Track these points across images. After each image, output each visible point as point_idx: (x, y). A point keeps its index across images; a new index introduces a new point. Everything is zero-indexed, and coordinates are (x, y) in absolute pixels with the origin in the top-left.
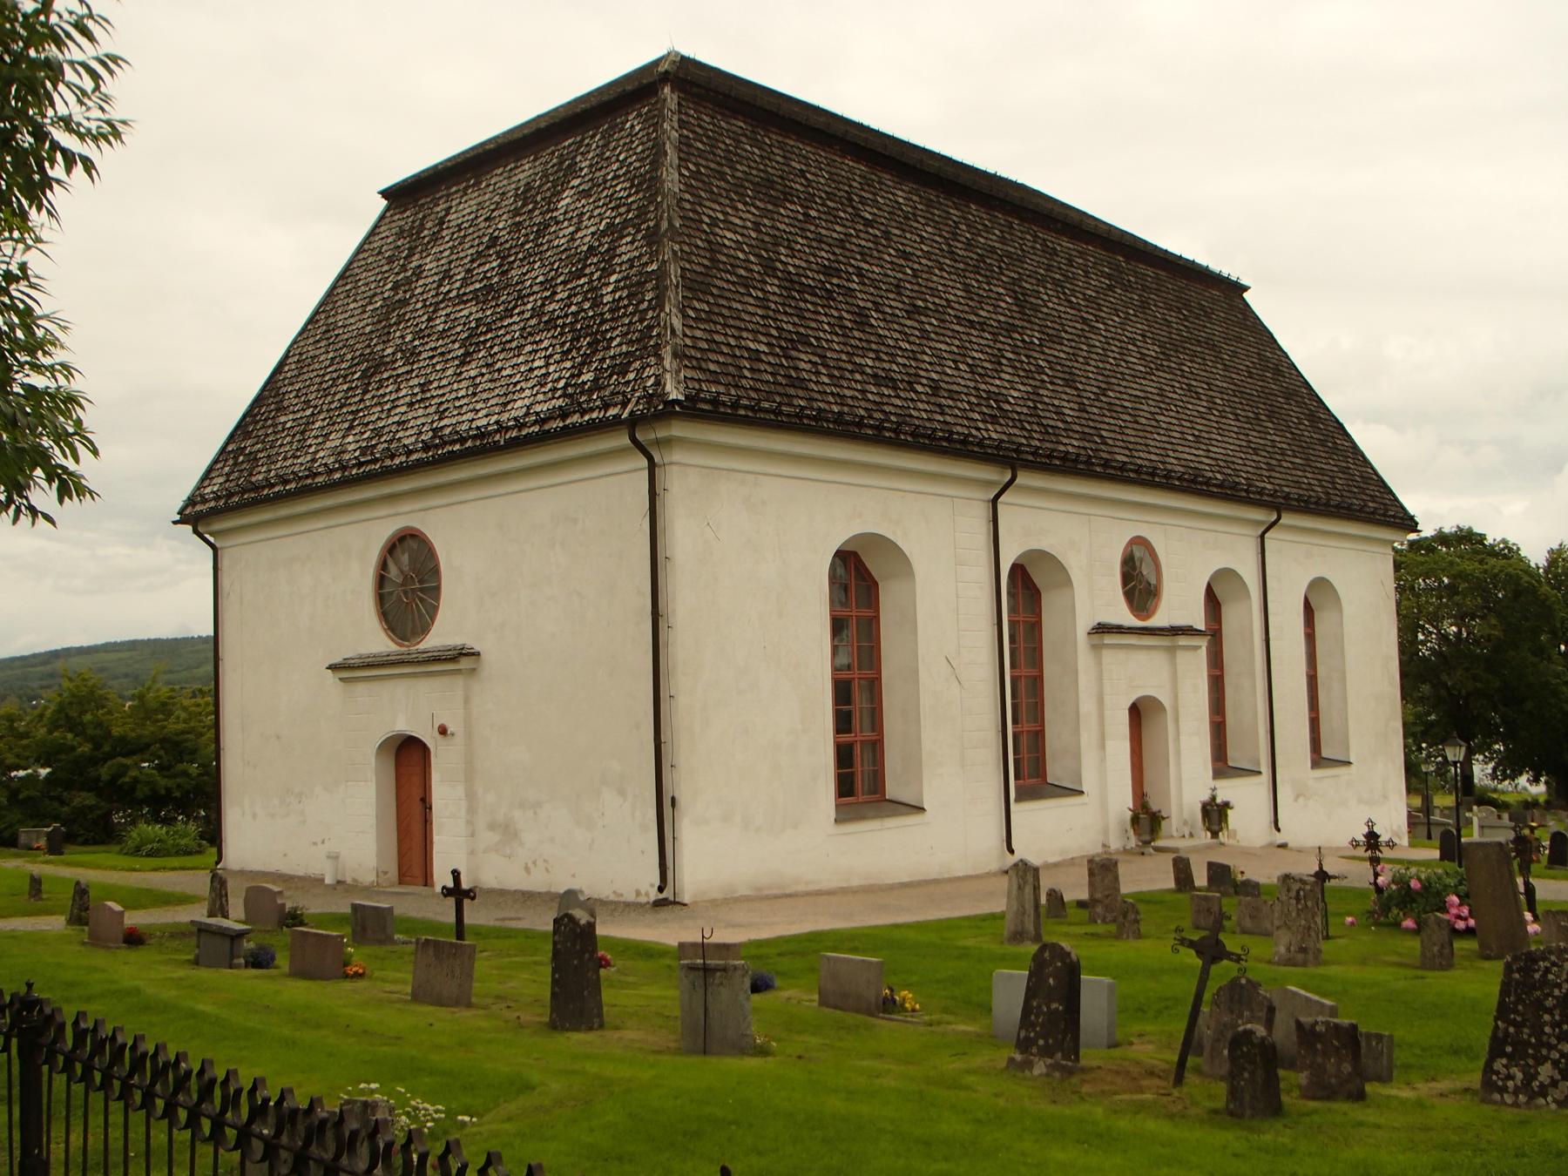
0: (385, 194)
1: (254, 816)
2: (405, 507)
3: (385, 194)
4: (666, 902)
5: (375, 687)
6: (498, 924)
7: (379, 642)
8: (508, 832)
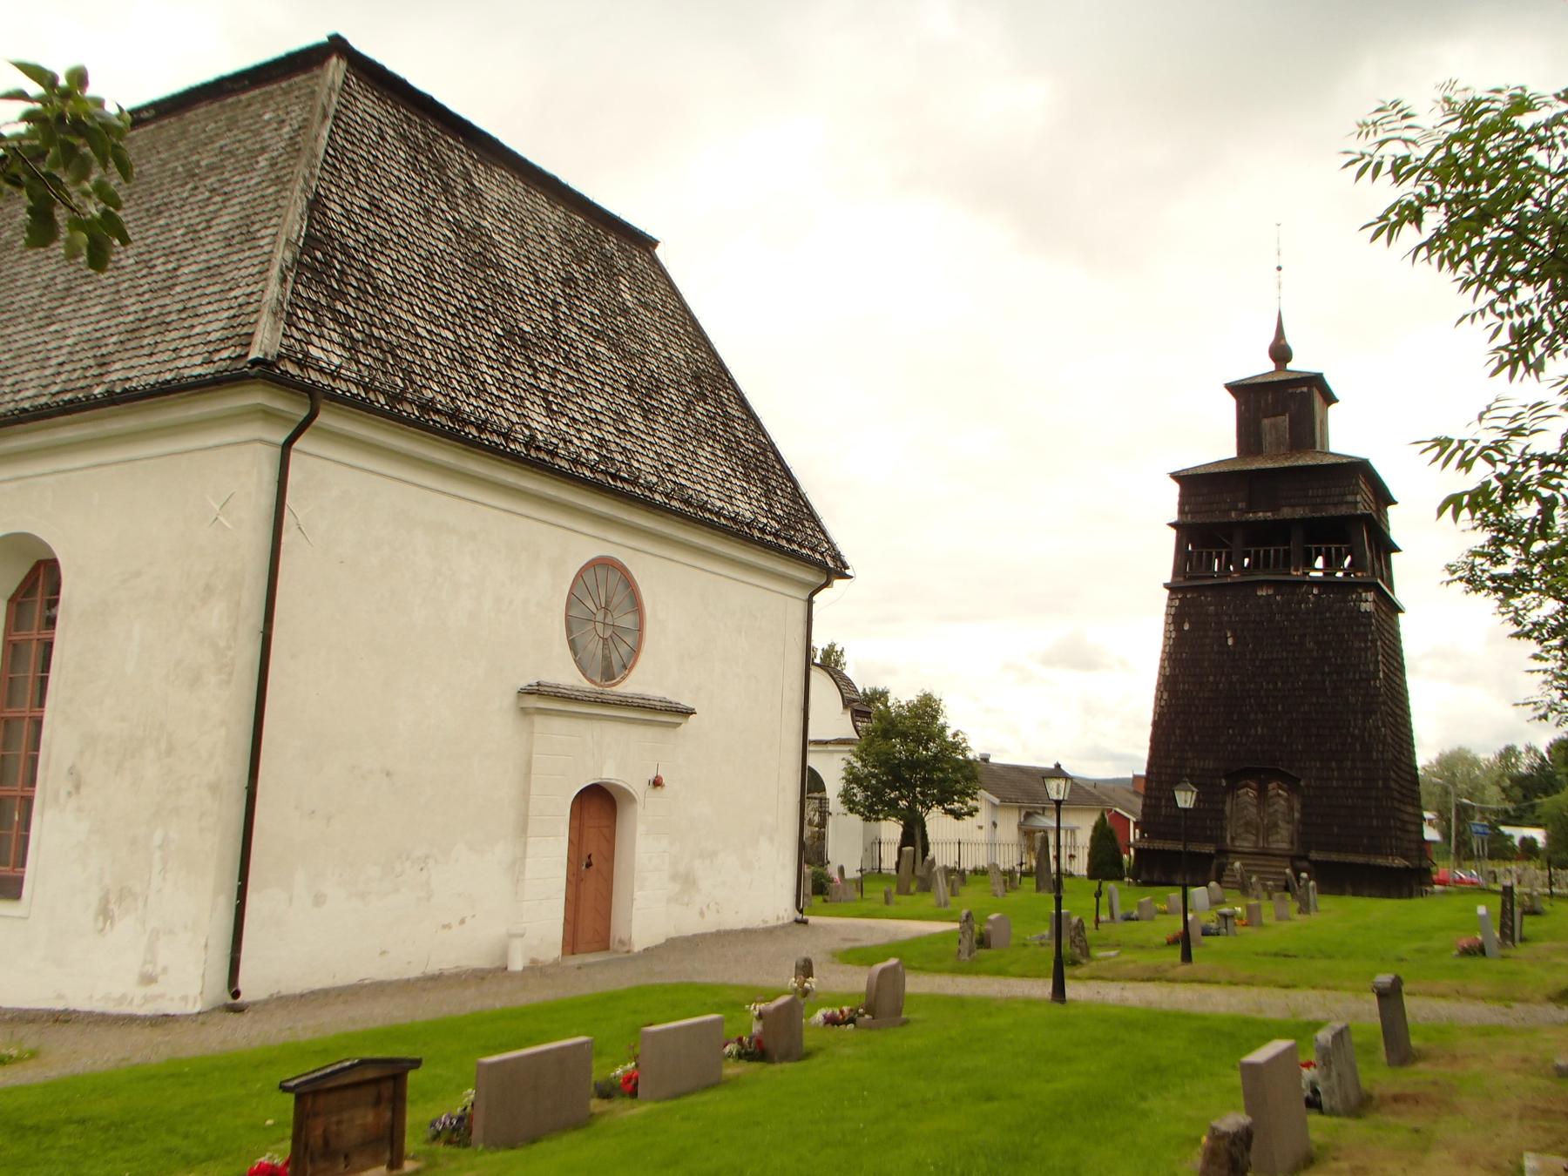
2: (615, 536)
4: (234, 1004)
6: (848, 945)
8: (687, 881)
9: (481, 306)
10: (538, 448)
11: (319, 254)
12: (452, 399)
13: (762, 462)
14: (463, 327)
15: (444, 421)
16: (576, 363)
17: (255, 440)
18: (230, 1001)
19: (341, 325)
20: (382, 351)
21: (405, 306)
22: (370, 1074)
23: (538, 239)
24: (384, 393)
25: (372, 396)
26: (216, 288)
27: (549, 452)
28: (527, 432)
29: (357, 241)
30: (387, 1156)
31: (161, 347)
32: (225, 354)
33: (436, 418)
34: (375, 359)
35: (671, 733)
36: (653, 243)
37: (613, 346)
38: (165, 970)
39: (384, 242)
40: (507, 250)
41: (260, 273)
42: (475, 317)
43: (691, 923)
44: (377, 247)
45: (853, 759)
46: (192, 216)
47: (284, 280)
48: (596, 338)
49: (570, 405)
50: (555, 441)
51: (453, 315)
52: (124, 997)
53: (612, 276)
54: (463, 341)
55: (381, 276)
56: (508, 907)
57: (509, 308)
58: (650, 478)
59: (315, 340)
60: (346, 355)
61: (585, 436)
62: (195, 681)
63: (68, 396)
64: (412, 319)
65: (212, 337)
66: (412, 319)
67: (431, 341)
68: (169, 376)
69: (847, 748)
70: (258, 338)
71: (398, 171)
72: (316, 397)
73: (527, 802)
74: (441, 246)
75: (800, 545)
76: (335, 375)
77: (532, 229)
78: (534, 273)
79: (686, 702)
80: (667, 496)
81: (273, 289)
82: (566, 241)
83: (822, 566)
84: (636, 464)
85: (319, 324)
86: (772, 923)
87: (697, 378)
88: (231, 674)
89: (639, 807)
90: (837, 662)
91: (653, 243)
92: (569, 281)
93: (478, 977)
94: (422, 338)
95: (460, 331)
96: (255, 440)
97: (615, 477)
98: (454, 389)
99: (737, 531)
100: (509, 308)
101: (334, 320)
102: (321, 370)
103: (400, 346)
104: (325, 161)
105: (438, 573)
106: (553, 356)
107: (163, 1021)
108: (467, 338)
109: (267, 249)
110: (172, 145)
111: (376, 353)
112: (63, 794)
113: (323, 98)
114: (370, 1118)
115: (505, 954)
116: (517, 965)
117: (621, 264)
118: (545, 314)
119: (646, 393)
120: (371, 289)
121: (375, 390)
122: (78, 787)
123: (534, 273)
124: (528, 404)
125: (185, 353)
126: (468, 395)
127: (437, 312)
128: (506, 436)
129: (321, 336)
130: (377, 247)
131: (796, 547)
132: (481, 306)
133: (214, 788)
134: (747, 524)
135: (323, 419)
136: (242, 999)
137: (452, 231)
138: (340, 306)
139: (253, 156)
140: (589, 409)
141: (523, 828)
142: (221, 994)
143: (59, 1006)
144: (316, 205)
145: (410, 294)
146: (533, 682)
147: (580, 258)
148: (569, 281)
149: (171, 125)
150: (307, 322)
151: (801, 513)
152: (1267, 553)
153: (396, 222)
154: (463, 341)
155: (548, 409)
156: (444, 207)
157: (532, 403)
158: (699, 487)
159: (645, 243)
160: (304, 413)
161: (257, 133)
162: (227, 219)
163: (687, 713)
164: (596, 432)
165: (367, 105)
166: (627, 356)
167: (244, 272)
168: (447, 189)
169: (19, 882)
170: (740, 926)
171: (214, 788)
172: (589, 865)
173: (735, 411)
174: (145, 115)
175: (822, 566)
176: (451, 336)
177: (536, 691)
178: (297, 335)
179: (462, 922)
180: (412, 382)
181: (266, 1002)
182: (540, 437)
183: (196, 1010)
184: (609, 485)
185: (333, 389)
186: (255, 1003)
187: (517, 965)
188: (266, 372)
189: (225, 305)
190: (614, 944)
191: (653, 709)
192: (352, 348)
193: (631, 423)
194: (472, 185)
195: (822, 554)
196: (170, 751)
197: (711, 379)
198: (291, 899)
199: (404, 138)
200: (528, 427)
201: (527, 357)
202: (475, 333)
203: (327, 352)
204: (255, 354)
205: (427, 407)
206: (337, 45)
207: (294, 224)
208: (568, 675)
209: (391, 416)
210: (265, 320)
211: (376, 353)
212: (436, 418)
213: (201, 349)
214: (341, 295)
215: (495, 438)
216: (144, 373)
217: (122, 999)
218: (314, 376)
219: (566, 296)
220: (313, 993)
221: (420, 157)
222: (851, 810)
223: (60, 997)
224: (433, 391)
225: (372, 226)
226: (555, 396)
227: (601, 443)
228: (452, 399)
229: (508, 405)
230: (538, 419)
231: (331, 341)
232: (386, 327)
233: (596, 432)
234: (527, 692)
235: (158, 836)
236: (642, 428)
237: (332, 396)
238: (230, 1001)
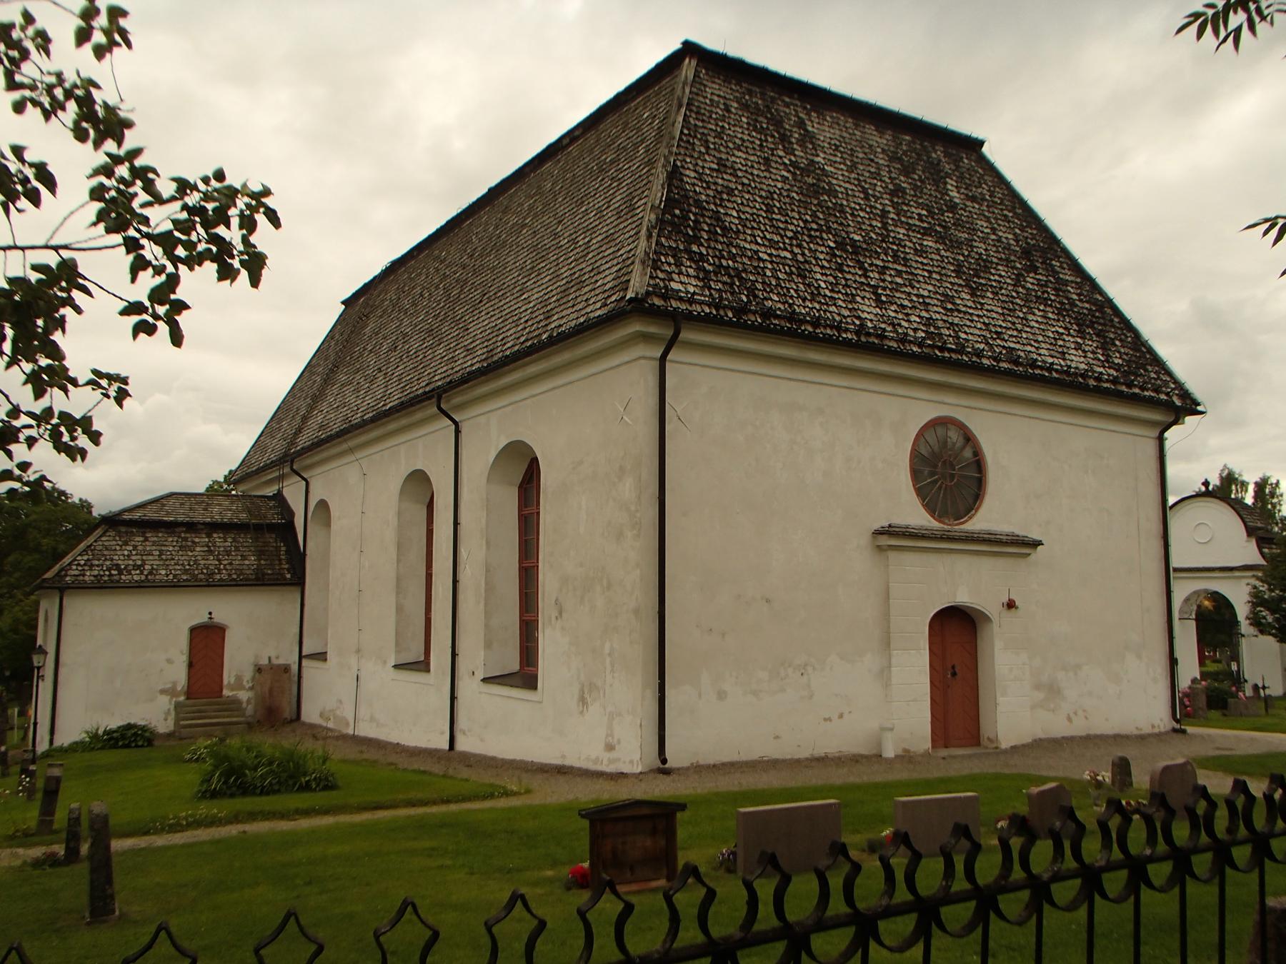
0: (343, 303)
1: (721, 695)
2: (951, 398)
3: (343, 303)
4: (663, 769)
5: (932, 558)
6: (1218, 753)
7: (916, 516)
8: (1052, 691)
9: (815, 226)
10: (868, 334)
11: (677, 212)
12: (790, 305)
13: (1099, 316)
14: (800, 246)
15: (783, 323)
16: (904, 259)
17: (640, 358)
19: (696, 262)
20: (730, 276)
21: (749, 238)
22: (646, 811)
23: (867, 162)
24: (732, 308)
25: (722, 313)
27: (877, 336)
28: (858, 322)
29: (707, 195)
30: (665, 872)
31: (579, 300)
32: (613, 298)
33: (776, 322)
34: (724, 283)
35: (1022, 562)
36: (981, 143)
37: (940, 239)
38: (619, 742)
39: (730, 192)
40: (840, 179)
42: (810, 236)
43: (1057, 726)
44: (725, 196)
45: (1258, 583)
46: (600, 202)
47: (649, 236)
49: (898, 295)
50: (883, 326)
51: (790, 238)
52: (597, 758)
53: (938, 178)
54: (800, 258)
55: (728, 219)
56: (885, 707)
57: (841, 224)
58: (977, 346)
59: (675, 277)
60: (700, 284)
61: (913, 318)
62: (620, 536)
63: (529, 344)
64: (754, 247)
65: (607, 287)
66: (754, 247)
67: (771, 262)
68: (582, 320)
69: (1249, 574)
70: (632, 283)
71: (740, 134)
72: (678, 320)
73: (889, 622)
74: (779, 185)
75: (1143, 389)
76: (691, 301)
77: (861, 155)
78: (864, 191)
79: (1035, 536)
80: (995, 359)
81: (643, 243)
82: (893, 158)
83: (1168, 406)
84: (963, 336)
85: (679, 264)
86: (1147, 730)
87: (1026, 253)
89: (995, 626)
90: (1273, 495)
91: (981, 143)
92: (897, 191)
93: (856, 759)
94: (764, 261)
95: (796, 250)
96: (640, 358)
97: (942, 349)
98: (792, 297)
99: (1072, 383)
100: (841, 224)
101: (690, 259)
102: (681, 299)
103: (745, 271)
104: (680, 139)
105: (831, 443)
106: (883, 257)
107: (622, 775)
108: (803, 254)
110: (591, 151)
111: (725, 279)
113: (679, 92)
114: (649, 843)
115: (879, 744)
116: (889, 753)
117: (947, 168)
118: (874, 223)
119: (974, 277)
120: (720, 227)
121: (725, 307)
122: (560, 613)
123: (864, 191)
124: (858, 299)
126: (804, 300)
127: (776, 238)
128: (838, 328)
129: (680, 273)
130: (725, 196)
131: (1137, 391)
132: (815, 226)
133: (636, 612)
134: (1082, 376)
135: (685, 335)
137: (789, 171)
138: (695, 248)
139: (636, 146)
140: (916, 295)
141: (886, 643)
143: (558, 762)
144: (674, 175)
145: (753, 228)
146: (886, 524)
147: (907, 171)
148: (897, 191)
149: (592, 137)
150: (669, 264)
151: (1143, 356)
153: (740, 174)
154: (800, 258)
155: (878, 300)
157: (863, 298)
158: (1029, 348)
160: (670, 333)
161: (639, 129)
163: (1036, 544)
164: (924, 314)
165: (715, 89)
166: (955, 245)
167: (627, 235)
168: (784, 139)
170: (1111, 732)
171: (636, 612)
172: (954, 674)
173: (1067, 276)
174: (577, 133)
175: (1168, 406)
176: (789, 256)
177: (889, 531)
178: (661, 275)
179: (841, 716)
180: (756, 296)
181: (688, 769)
182: (869, 324)
183: (639, 770)
184: (938, 357)
185: (691, 312)
186: (678, 769)
187: (889, 753)
189: (615, 262)
190: (984, 742)
191: (1006, 544)
192: (705, 277)
193: (958, 302)
194: (806, 130)
195: (1167, 394)
196: (609, 586)
197: (1041, 249)
198: (700, 695)
199: (745, 107)
200: (859, 318)
201: (858, 261)
202: (810, 249)
203: (685, 284)
204: (630, 295)
205: (768, 314)
206: (689, 49)
207: (657, 193)
208: (918, 517)
209: (740, 326)
210: (637, 267)
211: (725, 279)
212: (776, 322)
213: (600, 297)
214: (696, 239)
215: (829, 331)
216: (566, 319)
217: (596, 761)
218: (674, 304)
219: (894, 205)
220: (723, 764)
221: (761, 119)
222: (1262, 632)
223: (563, 757)
224: (774, 301)
225: (720, 181)
226: (884, 289)
227: (929, 322)
228: (790, 305)
229: (840, 303)
230: (868, 311)
231: (688, 276)
232: (733, 257)
233: (924, 314)
234: (879, 533)
235: (607, 646)
236: (970, 304)
237: (690, 318)
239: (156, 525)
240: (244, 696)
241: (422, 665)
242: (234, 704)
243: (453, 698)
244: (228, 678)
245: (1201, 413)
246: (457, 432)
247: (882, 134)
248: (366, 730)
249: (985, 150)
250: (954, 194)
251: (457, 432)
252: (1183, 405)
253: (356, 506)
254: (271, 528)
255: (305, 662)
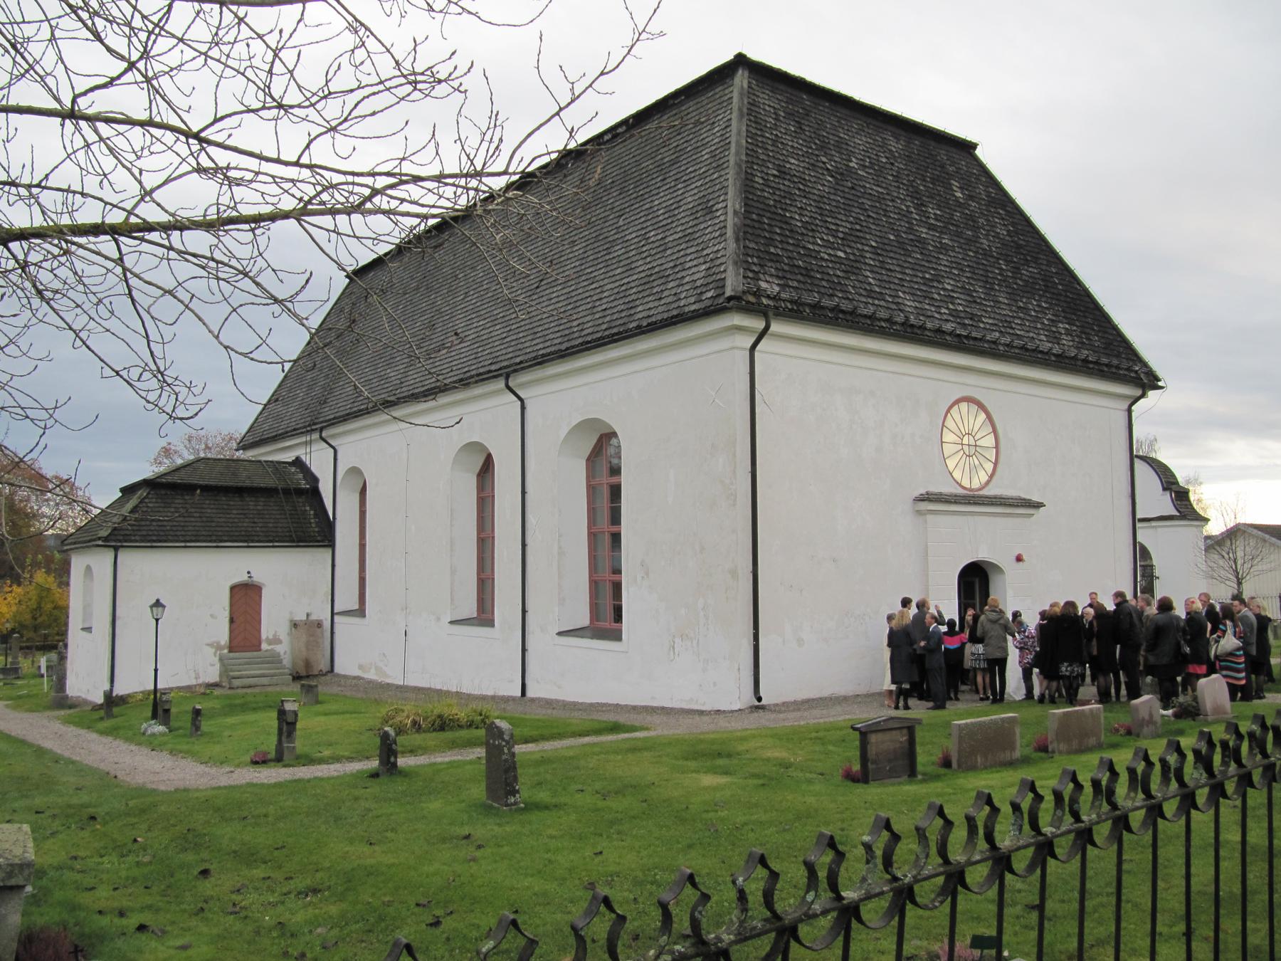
4: (758, 706)
18: (757, 703)
26: (693, 250)
32: (709, 294)
36: (973, 146)
41: (721, 235)
48: (941, 232)
66: (817, 248)
79: (1035, 498)
81: (732, 245)
88: (735, 500)
91: (973, 146)
102: (768, 297)
109: (722, 218)
112: (639, 579)
122: (647, 574)
125: (683, 296)
135: (776, 327)
136: (763, 702)
138: (772, 250)
142: (748, 699)
146: (923, 491)
152: (1239, 671)
156: (824, 159)
159: (967, 148)
162: (690, 199)
163: (1038, 505)
165: (768, 101)
169: (620, 631)
177: (928, 498)
188: (738, 304)
189: (701, 260)
203: (770, 286)
204: (728, 293)
206: (741, 61)
223: (653, 698)
238: (757, 703)
239: (189, 488)
240: (280, 649)
241: (484, 617)
242: (275, 659)
243: (524, 650)
244: (266, 632)
245: (1162, 388)
246: (523, 408)
247: (898, 139)
248: (413, 681)
249: (978, 152)
250: (959, 195)
251: (523, 408)
252: (1147, 381)
253: (397, 470)
254: (300, 492)
255: (336, 618)
